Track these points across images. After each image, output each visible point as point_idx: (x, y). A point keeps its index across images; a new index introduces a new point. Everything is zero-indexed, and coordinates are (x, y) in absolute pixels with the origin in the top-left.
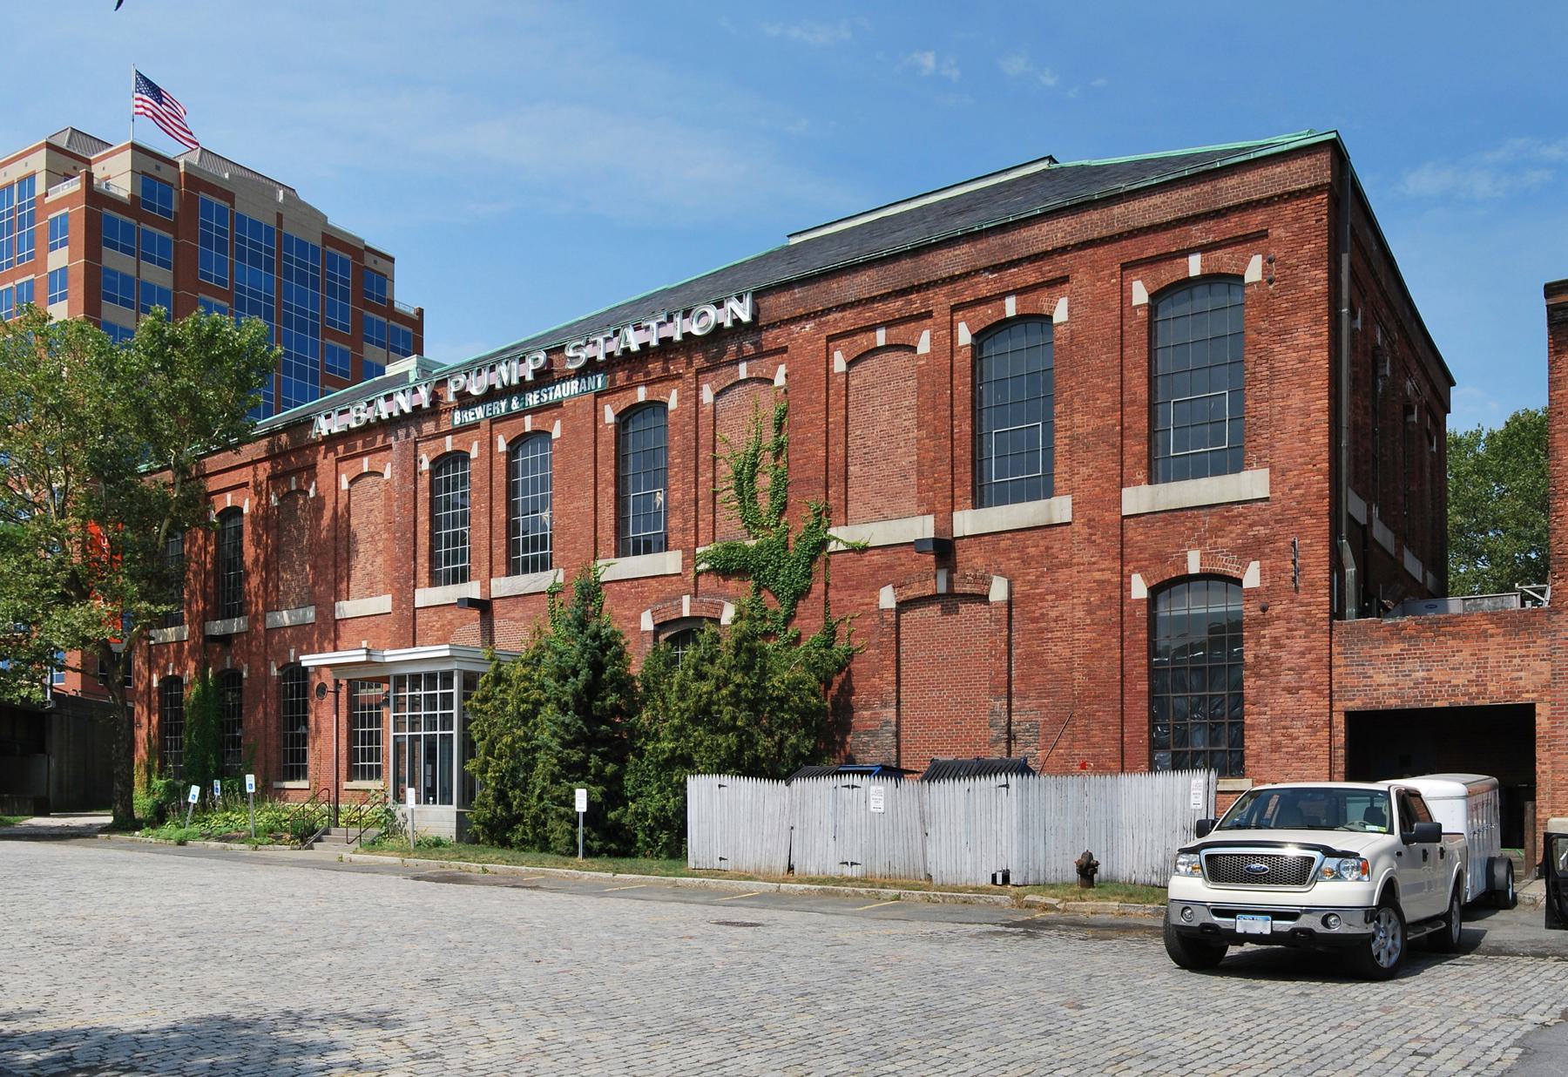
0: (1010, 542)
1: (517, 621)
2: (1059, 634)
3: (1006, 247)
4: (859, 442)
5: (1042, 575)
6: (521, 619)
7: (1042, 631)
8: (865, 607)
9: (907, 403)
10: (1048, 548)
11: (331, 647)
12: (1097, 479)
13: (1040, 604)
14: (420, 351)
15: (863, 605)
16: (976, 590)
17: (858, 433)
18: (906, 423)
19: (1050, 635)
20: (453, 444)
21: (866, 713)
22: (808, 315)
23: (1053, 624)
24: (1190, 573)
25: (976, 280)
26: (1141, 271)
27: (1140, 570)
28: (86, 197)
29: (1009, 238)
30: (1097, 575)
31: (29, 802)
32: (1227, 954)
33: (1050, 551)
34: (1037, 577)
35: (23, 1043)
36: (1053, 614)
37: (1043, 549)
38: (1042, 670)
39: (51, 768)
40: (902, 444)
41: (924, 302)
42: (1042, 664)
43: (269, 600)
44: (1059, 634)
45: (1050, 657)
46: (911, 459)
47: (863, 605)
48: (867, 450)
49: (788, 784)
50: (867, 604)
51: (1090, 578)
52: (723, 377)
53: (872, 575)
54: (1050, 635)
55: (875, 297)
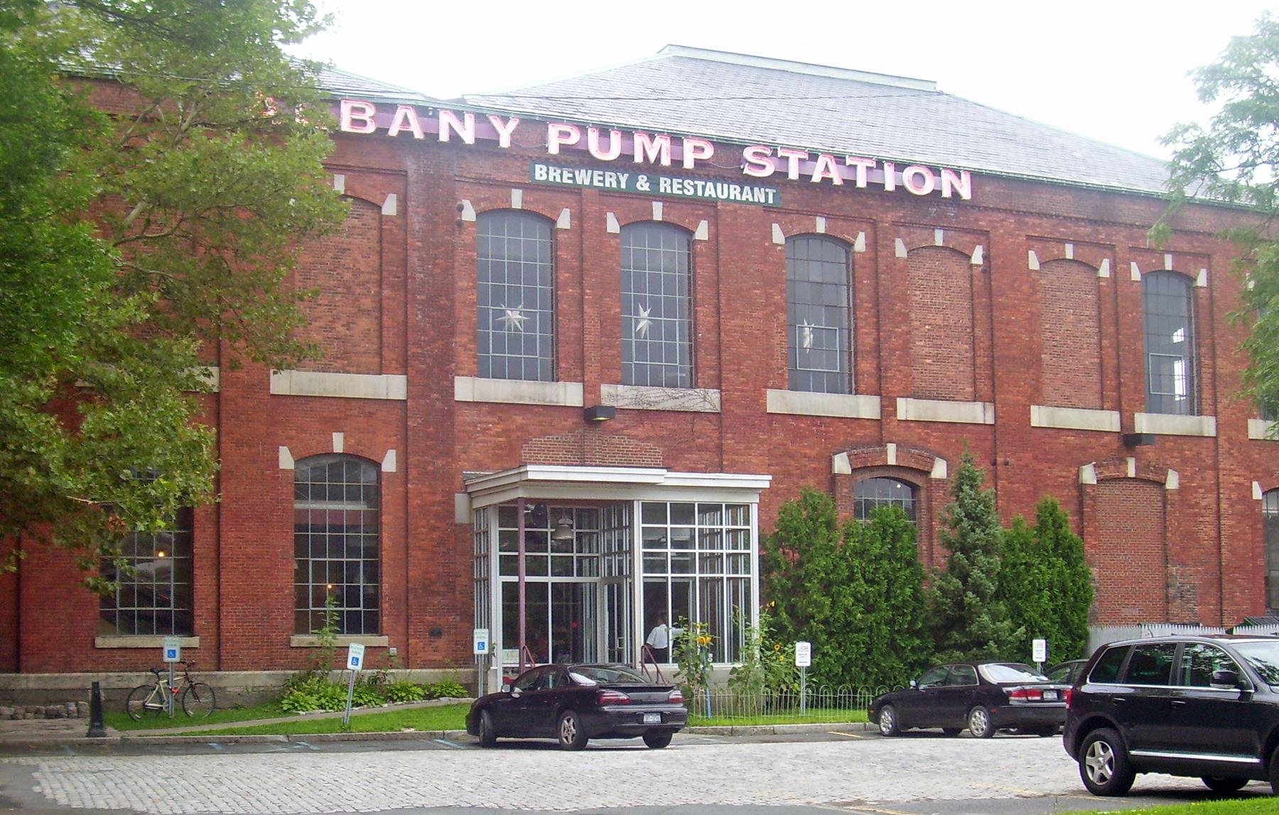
0: (1172, 444)
1: (642, 440)
2: (1207, 519)
3: (650, 696)
4: (1049, 334)
5: (1196, 473)
6: (648, 439)
7: (1196, 515)
8: (1062, 480)
9: (1088, 313)
10: (1198, 453)
11: (329, 111)
12: (1233, 408)
13: (1194, 495)
14: (809, 160)
15: (1060, 477)
16: (1157, 478)
17: (1047, 326)
18: (1088, 329)
19: (1201, 519)
20: (524, 201)
21: (81, 225)
22: (1011, 211)
23: (1203, 511)
24: (513, 207)
25: (690, 392)
26: (1037, 245)
27: (1257, 479)
28: (540, 749)
29: (587, 546)
30: (1236, 479)
31: (974, 628)
32: (1132, 788)
33: (1200, 456)
34: (1192, 474)
35: (663, 171)
36: (1203, 503)
37: (1195, 453)
38: (1197, 546)
39: (1247, 494)
40: (1085, 346)
41: (1109, 236)
42: (1197, 540)
43: (109, 10)
44: (1207, 519)
45: (1202, 535)
46: (1092, 360)
47: (1060, 477)
48: (1055, 343)
49: (1202, 432)
50: (1064, 477)
51: (1230, 480)
52: (919, 236)
53: (1069, 453)
54: (1201, 519)
55: (1071, 218)
